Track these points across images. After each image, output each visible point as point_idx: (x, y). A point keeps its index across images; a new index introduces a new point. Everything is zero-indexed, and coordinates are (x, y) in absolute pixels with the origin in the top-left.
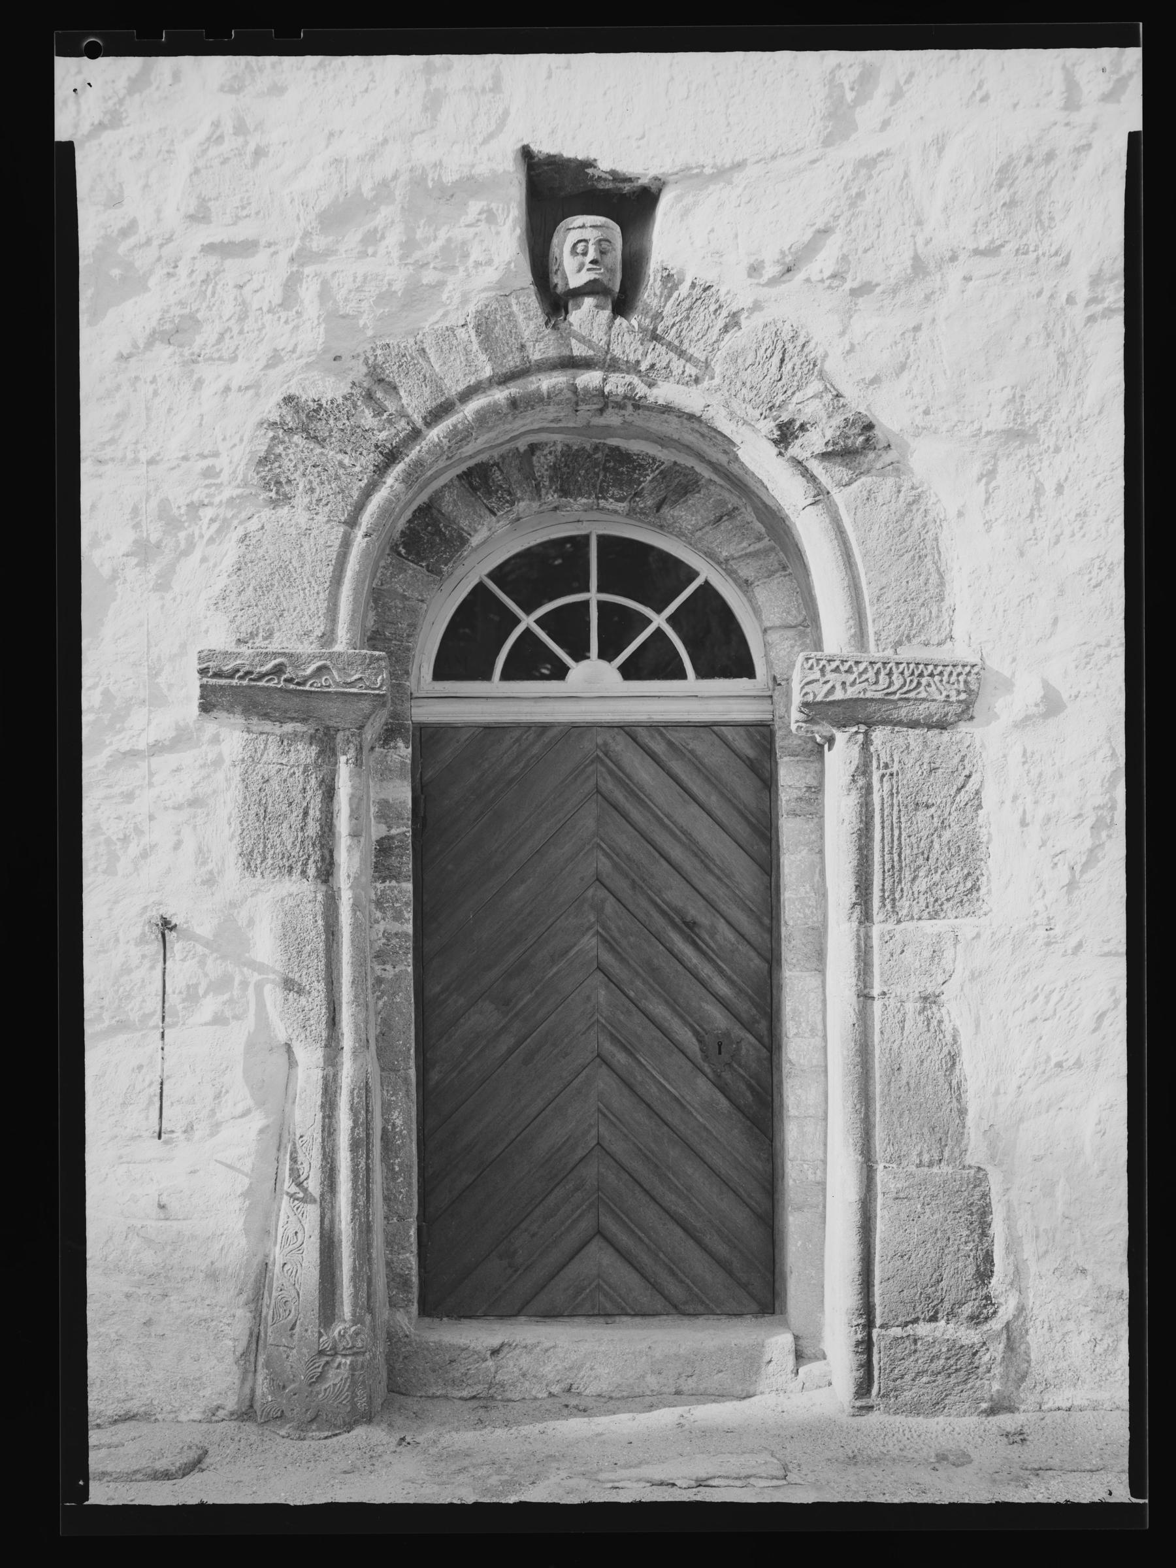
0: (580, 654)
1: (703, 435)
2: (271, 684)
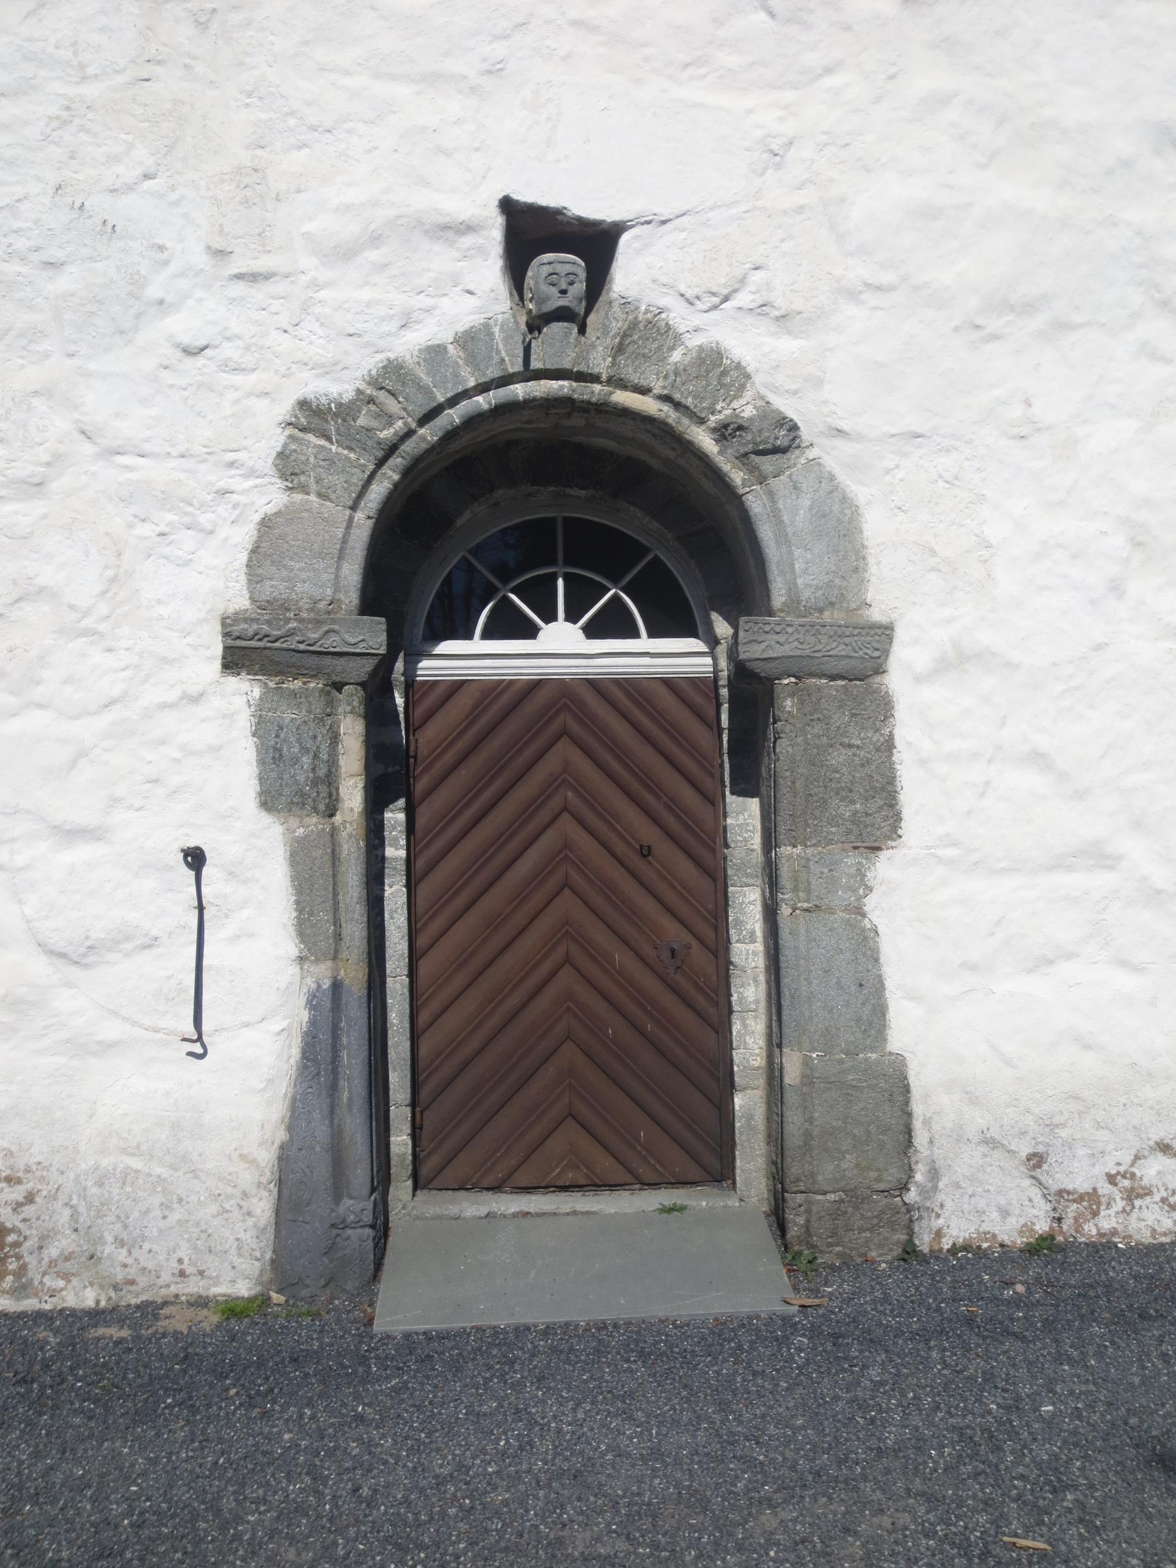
0: (550, 617)
1: (654, 435)
2: (284, 645)
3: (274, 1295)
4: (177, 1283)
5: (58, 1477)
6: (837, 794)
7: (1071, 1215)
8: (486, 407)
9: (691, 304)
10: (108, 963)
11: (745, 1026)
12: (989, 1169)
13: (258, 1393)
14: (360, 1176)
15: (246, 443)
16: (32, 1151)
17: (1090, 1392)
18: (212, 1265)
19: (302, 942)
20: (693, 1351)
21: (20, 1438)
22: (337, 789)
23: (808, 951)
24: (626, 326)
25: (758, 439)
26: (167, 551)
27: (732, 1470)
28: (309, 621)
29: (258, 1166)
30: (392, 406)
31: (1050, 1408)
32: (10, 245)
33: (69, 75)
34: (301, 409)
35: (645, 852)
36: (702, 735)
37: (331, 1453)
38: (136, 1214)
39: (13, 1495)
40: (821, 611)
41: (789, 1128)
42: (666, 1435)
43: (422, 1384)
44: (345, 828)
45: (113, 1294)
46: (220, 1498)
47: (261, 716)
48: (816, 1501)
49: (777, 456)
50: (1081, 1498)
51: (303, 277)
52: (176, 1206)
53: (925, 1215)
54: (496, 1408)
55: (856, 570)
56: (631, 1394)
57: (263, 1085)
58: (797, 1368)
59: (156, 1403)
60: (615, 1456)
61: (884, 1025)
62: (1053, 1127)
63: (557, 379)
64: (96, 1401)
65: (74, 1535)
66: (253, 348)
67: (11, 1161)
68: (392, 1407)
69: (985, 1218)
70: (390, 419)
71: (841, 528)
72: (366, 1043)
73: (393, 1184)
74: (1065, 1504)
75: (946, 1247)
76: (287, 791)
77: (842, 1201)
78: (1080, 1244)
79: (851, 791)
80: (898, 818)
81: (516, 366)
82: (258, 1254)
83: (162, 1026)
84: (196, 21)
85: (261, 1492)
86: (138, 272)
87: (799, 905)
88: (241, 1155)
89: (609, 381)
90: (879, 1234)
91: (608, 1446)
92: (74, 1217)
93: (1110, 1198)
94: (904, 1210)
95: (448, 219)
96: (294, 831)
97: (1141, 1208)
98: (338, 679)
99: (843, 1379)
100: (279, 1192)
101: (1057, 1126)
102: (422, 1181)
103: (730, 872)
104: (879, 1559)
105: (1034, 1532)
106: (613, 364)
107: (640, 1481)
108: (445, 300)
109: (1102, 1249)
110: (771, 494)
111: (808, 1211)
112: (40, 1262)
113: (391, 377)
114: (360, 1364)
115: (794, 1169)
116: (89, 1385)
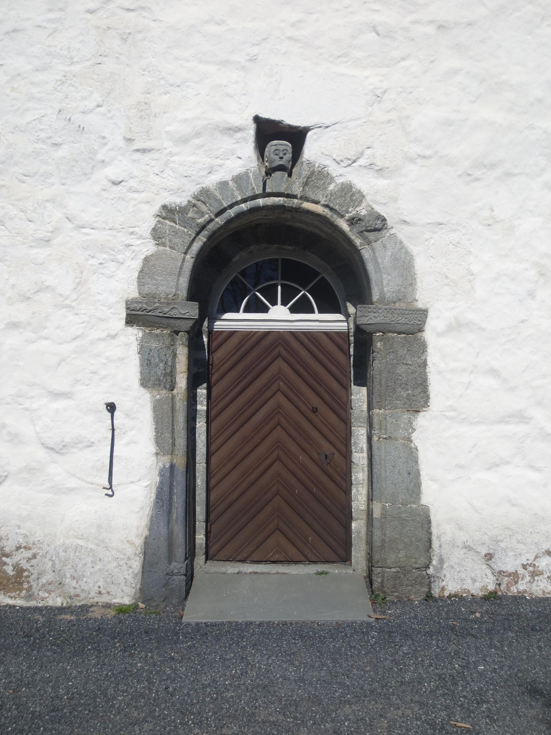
0: (274, 303)
1: (322, 222)
2: (153, 314)
3: (140, 604)
4: (97, 597)
5: (38, 677)
6: (400, 386)
7: (505, 582)
8: (245, 209)
9: (339, 164)
10: (71, 453)
11: (358, 491)
12: (467, 560)
13: (129, 646)
14: (180, 552)
15: (139, 224)
16: (36, 535)
17: (502, 662)
18: (113, 589)
19: (158, 446)
20: (325, 636)
21: (23, 660)
22: (175, 378)
23: (385, 457)
24: (309, 173)
25: (368, 225)
26: (103, 271)
27: (334, 688)
28: (164, 303)
29: (135, 546)
30: (204, 208)
31: (482, 667)
32: (38, 136)
33: (66, 62)
34: (163, 209)
35: (315, 410)
36: (341, 358)
37: (158, 673)
38: (80, 565)
39: (18, 684)
40: (395, 303)
41: (375, 538)
42: (307, 672)
43: (201, 645)
44: (178, 396)
45: (69, 601)
46: (107, 689)
47: (142, 345)
48: (370, 703)
49: (376, 232)
50: (490, 707)
51: (166, 150)
52: (98, 562)
53: (437, 580)
54: (233, 657)
55: (411, 284)
56: (294, 653)
57: (138, 510)
58: (370, 645)
59: (84, 648)
60: (283, 680)
61: (420, 492)
62: (497, 541)
63: (278, 197)
64: (58, 646)
65: (42, 701)
66: (143, 182)
67: (26, 540)
68: (187, 654)
69: (465, 582)
70: (203, 214)
71: (405, 265)
72: (185, 492)
73: (196, 557)
74: (482, 709)
75: (446, 595)
76: (152, 379)
77: (398, 572)
78: (509, 596)
79: (407, 385)
80: (428, 397)
81: (259, 191)
82: (134, 586)
83: (95, 482)
84: (122, 38)
85: (125, 687)
86: (93, 148)
87: (382, 436)
88: (128, 541)
89: (301, 198)
90: (415, 588)
91: (281, 675)
92: (53, 565)
93: (523, 576)
94: (427, 577)
95: (230, 125)
96: (155, 397)
97: (538, 580)
98: (177, 329)
99: (391, 651)
100: (144, 558)
101: (499, 541)
102: (210, 556)
103: (352, 420)
104: (394, 729)
105: (466, 720)
106: (303, 190)
107: (293, 691)
108: (228, 161)
109: (519, 599)
110: (373, 250)
111: (383, 576)
112: (38, 585)
113: (204, 195)
114: (175, 635)
115: (377, 557)
116: (55, 639)
